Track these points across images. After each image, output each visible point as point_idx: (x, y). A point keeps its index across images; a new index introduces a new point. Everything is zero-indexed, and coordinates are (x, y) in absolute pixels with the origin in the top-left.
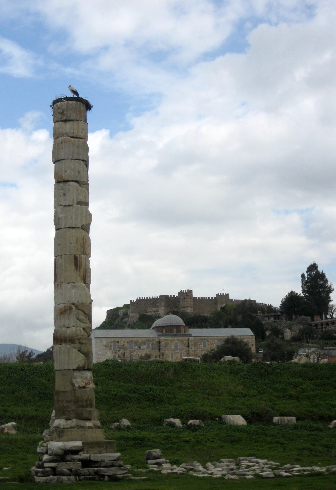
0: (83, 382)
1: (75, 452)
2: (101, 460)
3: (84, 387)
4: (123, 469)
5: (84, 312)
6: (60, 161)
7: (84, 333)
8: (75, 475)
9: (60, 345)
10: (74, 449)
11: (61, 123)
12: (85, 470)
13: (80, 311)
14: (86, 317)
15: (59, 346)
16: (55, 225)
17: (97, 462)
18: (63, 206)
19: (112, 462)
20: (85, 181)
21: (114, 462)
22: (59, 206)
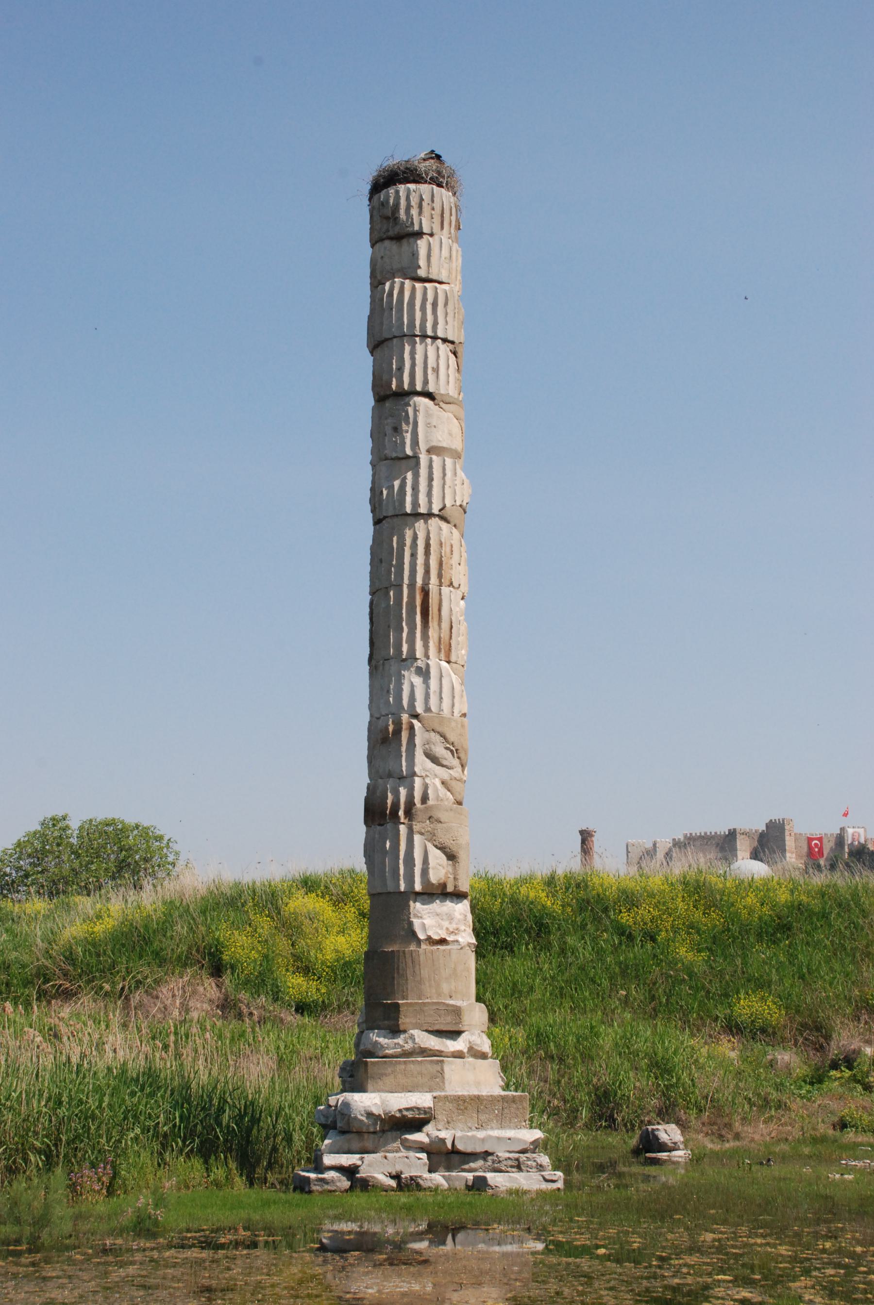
0: (440, 927)
3: (443, 941)
4: (547, 1177)
5: (443, 736)
6: (385, 343)
7: (446, 795)
9: (380, 825)
11: (387, 243)
12: (438, 1178)
13: (432, 734)
14: (452, 751)
15: (378, 828)
16: (373, 511)
17: (472, 1156)
18: (392, 459)
19: (517, 1155)
20: (451, 394)
21: (521, 1155)
22: (381, 460)
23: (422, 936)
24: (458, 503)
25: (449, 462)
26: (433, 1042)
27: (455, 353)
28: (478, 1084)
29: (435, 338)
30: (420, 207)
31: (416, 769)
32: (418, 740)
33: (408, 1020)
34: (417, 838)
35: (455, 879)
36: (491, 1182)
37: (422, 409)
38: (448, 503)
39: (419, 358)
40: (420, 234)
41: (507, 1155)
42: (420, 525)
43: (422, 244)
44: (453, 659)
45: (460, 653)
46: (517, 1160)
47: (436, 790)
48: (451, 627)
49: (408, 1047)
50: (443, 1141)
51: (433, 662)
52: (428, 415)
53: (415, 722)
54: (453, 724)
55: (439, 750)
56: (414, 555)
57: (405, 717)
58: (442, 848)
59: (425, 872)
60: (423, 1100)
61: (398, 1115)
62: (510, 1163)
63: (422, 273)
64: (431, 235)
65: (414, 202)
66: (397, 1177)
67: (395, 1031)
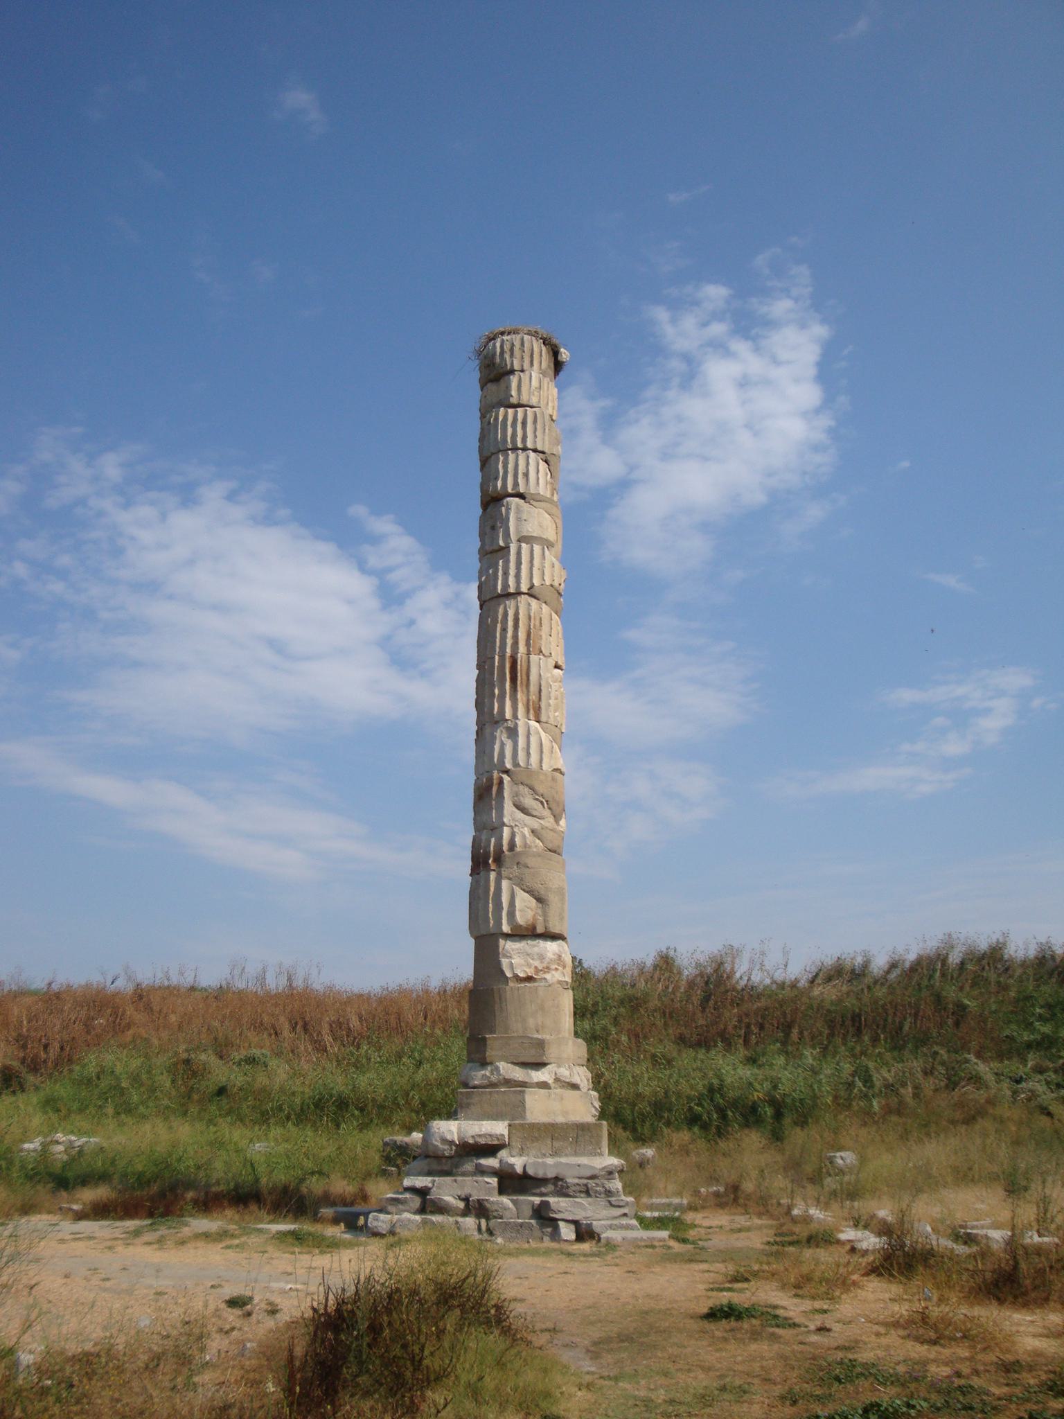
0: (529, 965)
1: (491, 1150)
2: (553, 1175)
3: (529, 979)
8: (478, 1216)
10: (482, 1141)
13: (521, 787)
17: (544, 1181)
19: (585, 1181)
23: (509, 974)
24: (548, 583)
25: (537, 548)
26: (518, 1074)
27: (546, 461)
28: (565, 1113)
29: (525, 449)
30: (512, 350)
31: (505, 820)
32: (506, 794)
33: (493, 1053)
34: (505, 884)
35: (545, 921)
36: (553, 1206)
37: (513, 507)
38: (536, 582)
39: (511, 466)
40: (512, 372)
41: (576, 1181)
42: (511, 604)
43: (514, 380)
44: (543, 718)
45: (552, 713)
46: (586, 1185)
47: (524, 837)
48: (540, 691)
49: (494, 1078)
50: (512, 1166)
51: (521, 723)
52: (518, 510)
53: (506, 778)
54: (542, 777)
55: (528, 801)
56: (504, 630)
57: (495, 774)
58: (530, 892)
59: (511, 914)
60: (499, 1128)
61: (471, 1141)
62: (578, 1188)
63: (514, 400)
64: (522, 371)
65: (507, 348)
66: (466, 1199)
67: (484, 1063)
